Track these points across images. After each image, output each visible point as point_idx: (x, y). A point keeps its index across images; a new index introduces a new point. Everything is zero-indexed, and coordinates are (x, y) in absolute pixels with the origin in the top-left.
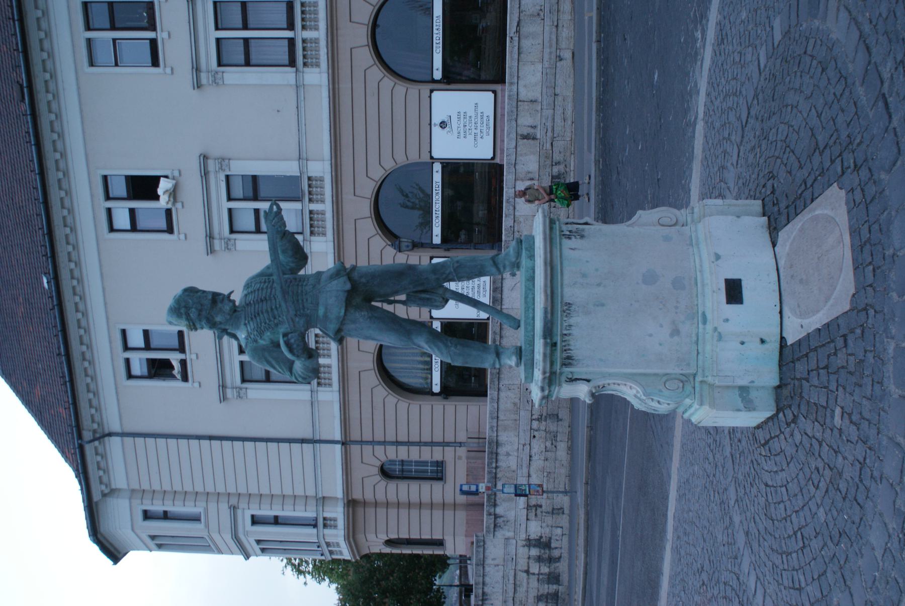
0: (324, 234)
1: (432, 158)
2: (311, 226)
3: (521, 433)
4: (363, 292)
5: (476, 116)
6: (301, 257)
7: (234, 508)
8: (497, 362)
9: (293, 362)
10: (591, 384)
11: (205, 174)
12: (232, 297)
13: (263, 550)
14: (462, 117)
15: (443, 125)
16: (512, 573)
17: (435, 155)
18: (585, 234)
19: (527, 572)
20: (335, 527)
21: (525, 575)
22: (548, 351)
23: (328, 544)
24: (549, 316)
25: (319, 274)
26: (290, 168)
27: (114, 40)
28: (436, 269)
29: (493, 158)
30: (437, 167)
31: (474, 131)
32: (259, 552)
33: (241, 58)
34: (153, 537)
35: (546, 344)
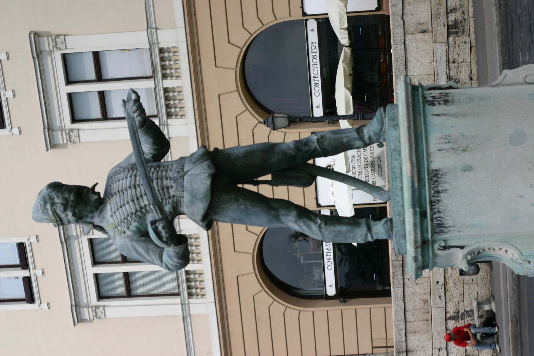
1: (304, 14)
2: (168, 106)
3: (435, 335)
4: (230, 177)
6: (162, 144)
8: (369, 235)
9: (163, 249)
10: (466, 251)
11: (38, 55)
12: (96, 190)
17: (308, 11)
18: (450, 99)
22: (418, 221)
24: (416, 184)
25: (182, 159)
28: (300, 144)
29: (377, 9)
30: (312, 25)
35: (415, 213)
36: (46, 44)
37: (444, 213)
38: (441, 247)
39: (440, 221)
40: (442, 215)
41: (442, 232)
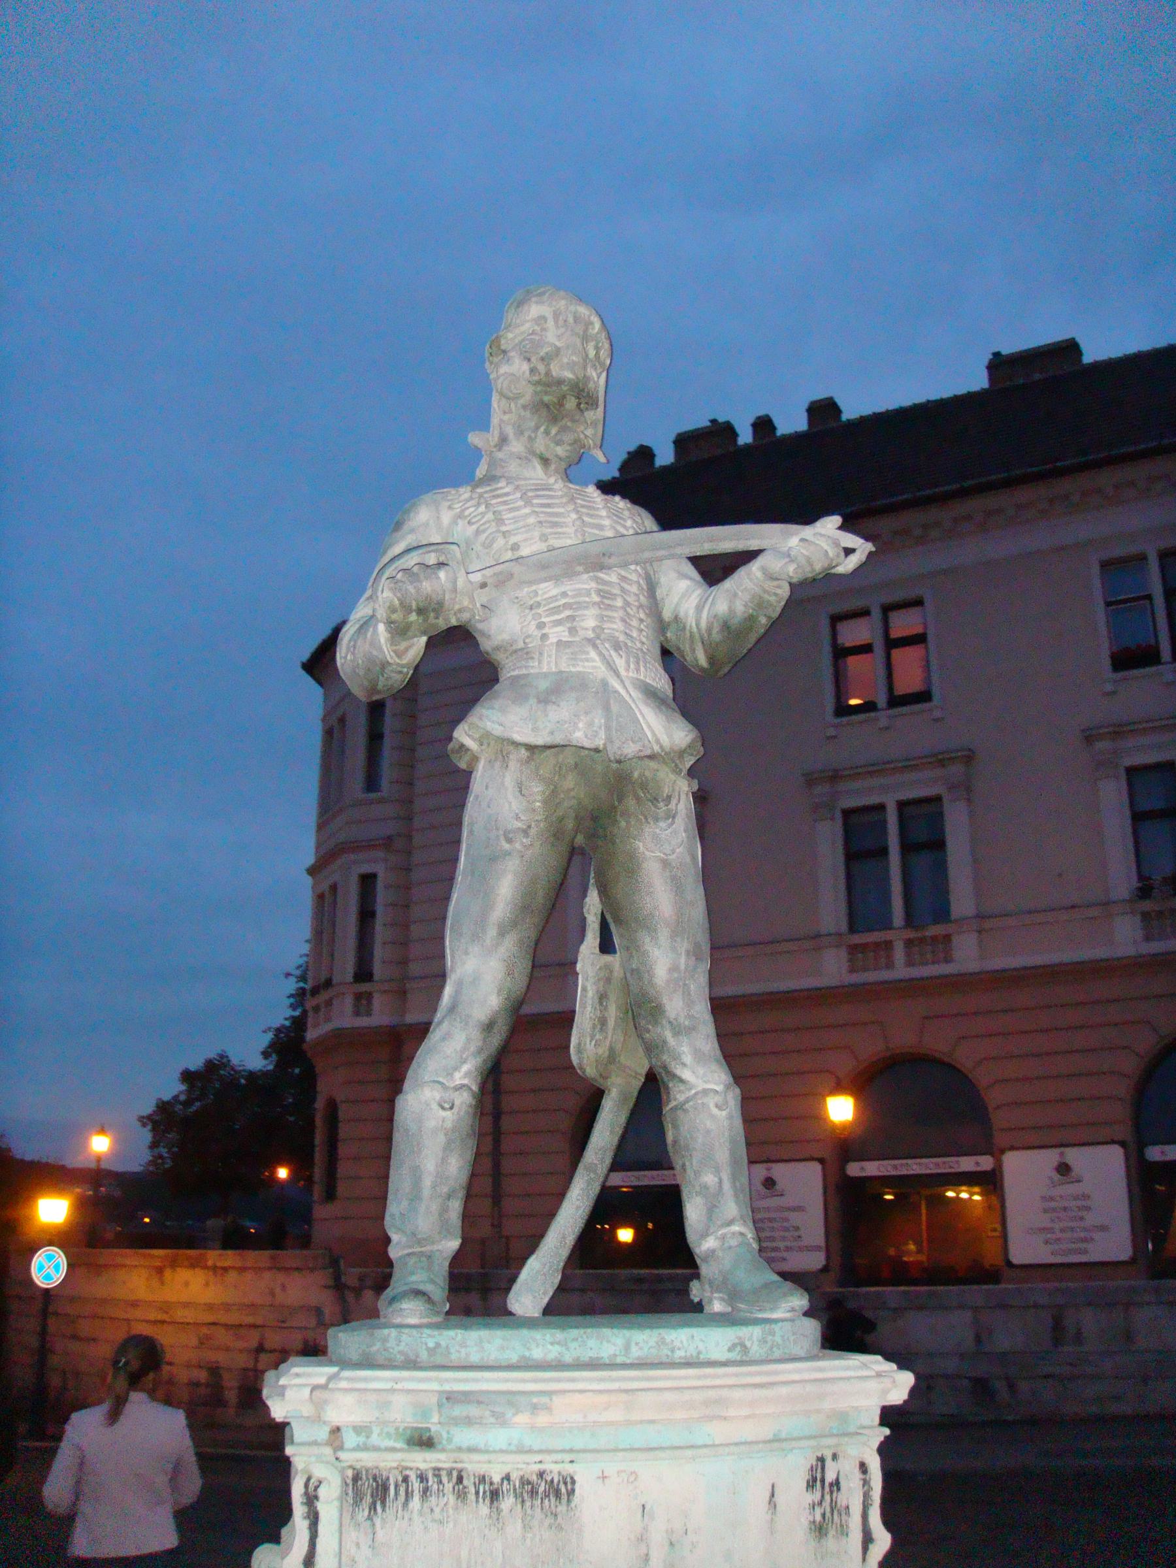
0: (852, 970)
1: (1002, 1151)
5: (1085, 1229)
7: (387, 843)
11: (940, 760)
13: (321, 897)
14: (1080, 1203)
15: (1064, 1169)
16: (259, 1322)
18: (830, 1542)
19: (260, 1349)
20: (357, 1013)
21: (254, 1343)
23: (329, 1003)
26: (962, 902)
27: (1149, 597)
31: (1057, 1226)
32: (319, 891)
33: (1144, 805)
34: (342, 720)
36: (956, 769)
37: (421, 1513)
38: (316, 1488)
39: (396, 1494)
40: (416, 1502)
41: (358, 1498)
